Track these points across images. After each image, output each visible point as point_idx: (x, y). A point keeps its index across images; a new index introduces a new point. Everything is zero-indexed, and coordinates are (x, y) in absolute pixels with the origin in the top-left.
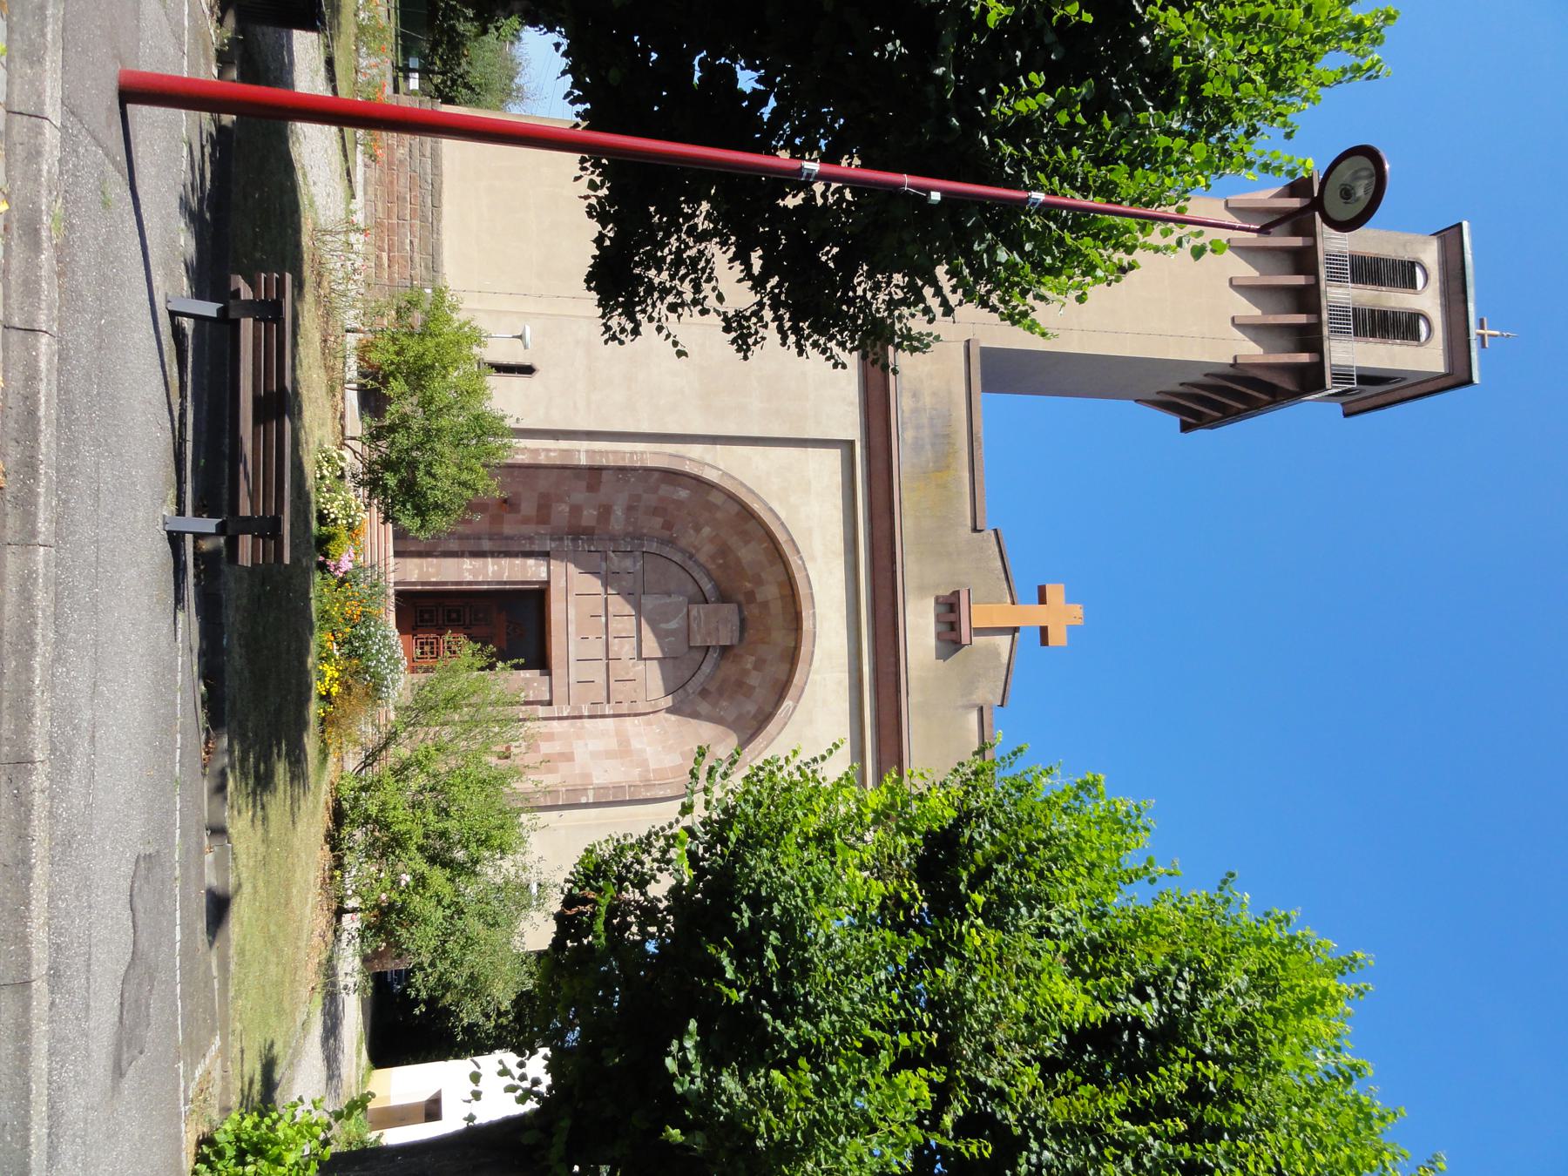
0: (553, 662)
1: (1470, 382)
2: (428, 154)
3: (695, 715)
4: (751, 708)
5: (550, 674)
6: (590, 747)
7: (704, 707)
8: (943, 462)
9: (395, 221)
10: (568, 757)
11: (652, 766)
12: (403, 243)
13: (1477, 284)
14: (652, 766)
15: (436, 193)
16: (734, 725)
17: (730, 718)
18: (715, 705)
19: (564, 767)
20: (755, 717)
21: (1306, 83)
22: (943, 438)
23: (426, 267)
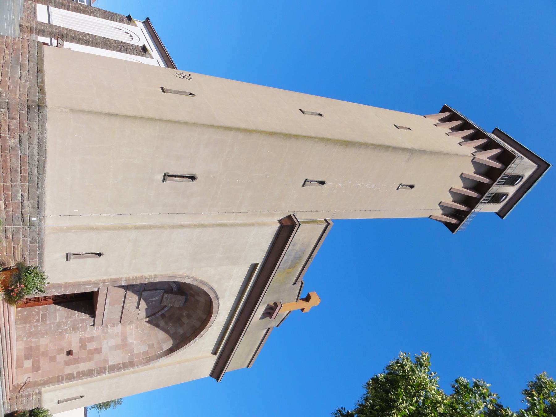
0: (97, 313)
1: (502, 218)
2: (35, 142)
3: (157, 326)
4: (181, 331)
5: (94, 317)
6: (109, 344)
7: (162, 323)
8: (293, 266)
9: (9, 184)
10: (98, 351)
11: (135, 352)
12: (16, 196)
13: (538, 183)
14: (135, 352)
15: (41, 166)
16: (173, 336)
17: (172, 332)
18: (166, 323)
19: (97, 357)
20: (181, 336)
21: (424, 392)
22: (298, 258)
23: (33, 208)
